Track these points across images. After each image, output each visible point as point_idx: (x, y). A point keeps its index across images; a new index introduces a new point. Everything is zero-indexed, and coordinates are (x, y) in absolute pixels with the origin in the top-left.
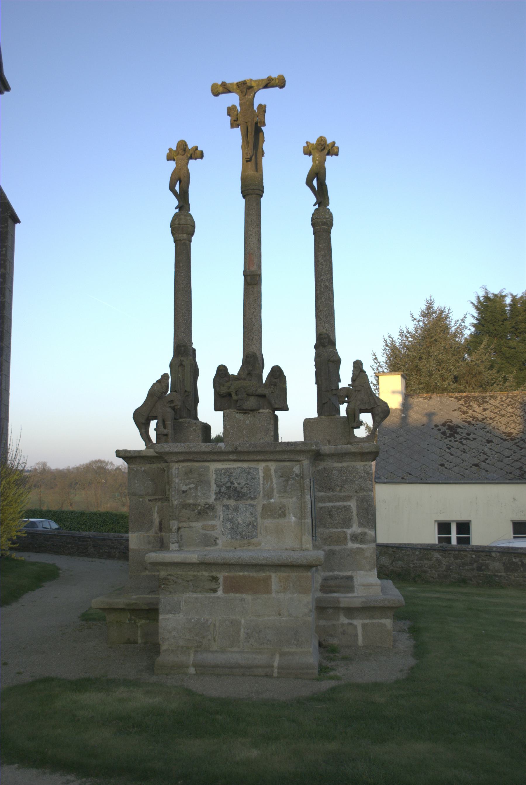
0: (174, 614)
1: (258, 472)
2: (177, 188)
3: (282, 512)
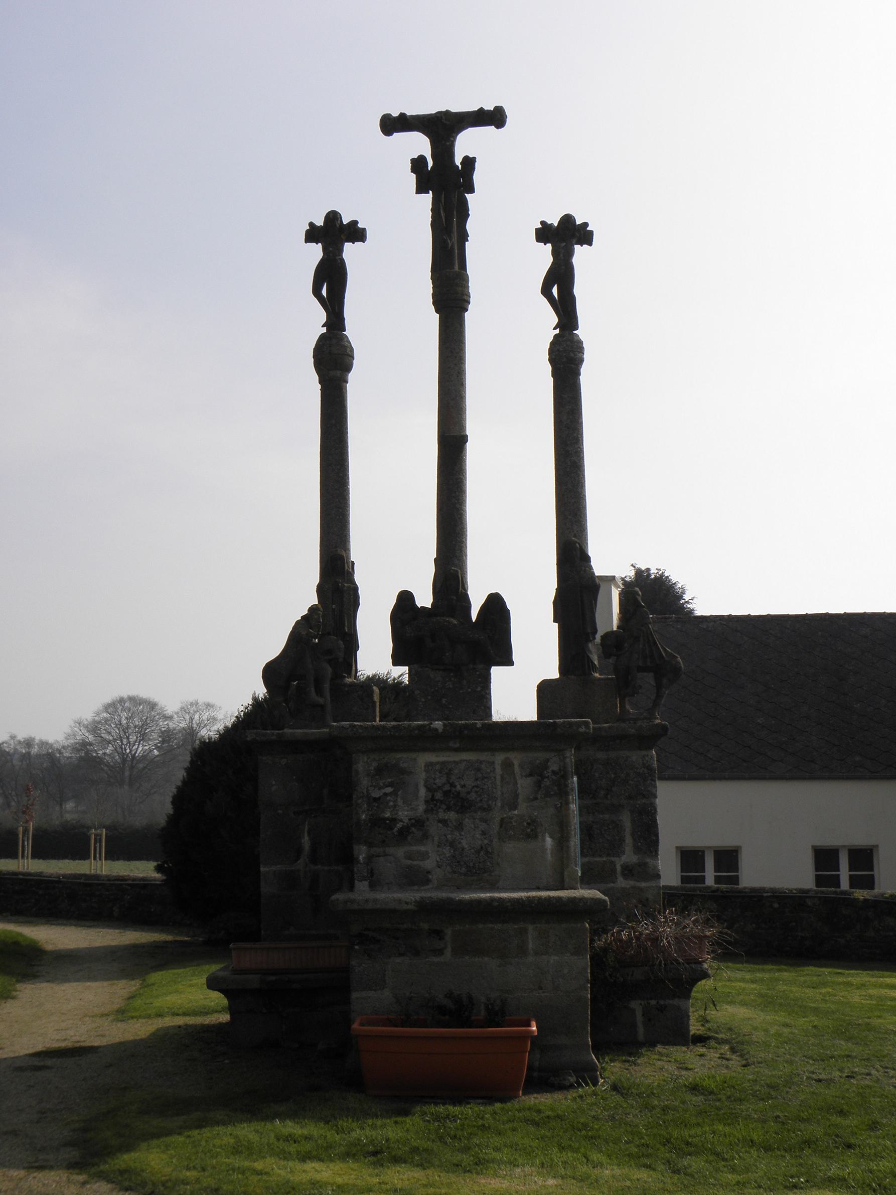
0: (375, 990)
1: (495, 769)
2: (324, 292)
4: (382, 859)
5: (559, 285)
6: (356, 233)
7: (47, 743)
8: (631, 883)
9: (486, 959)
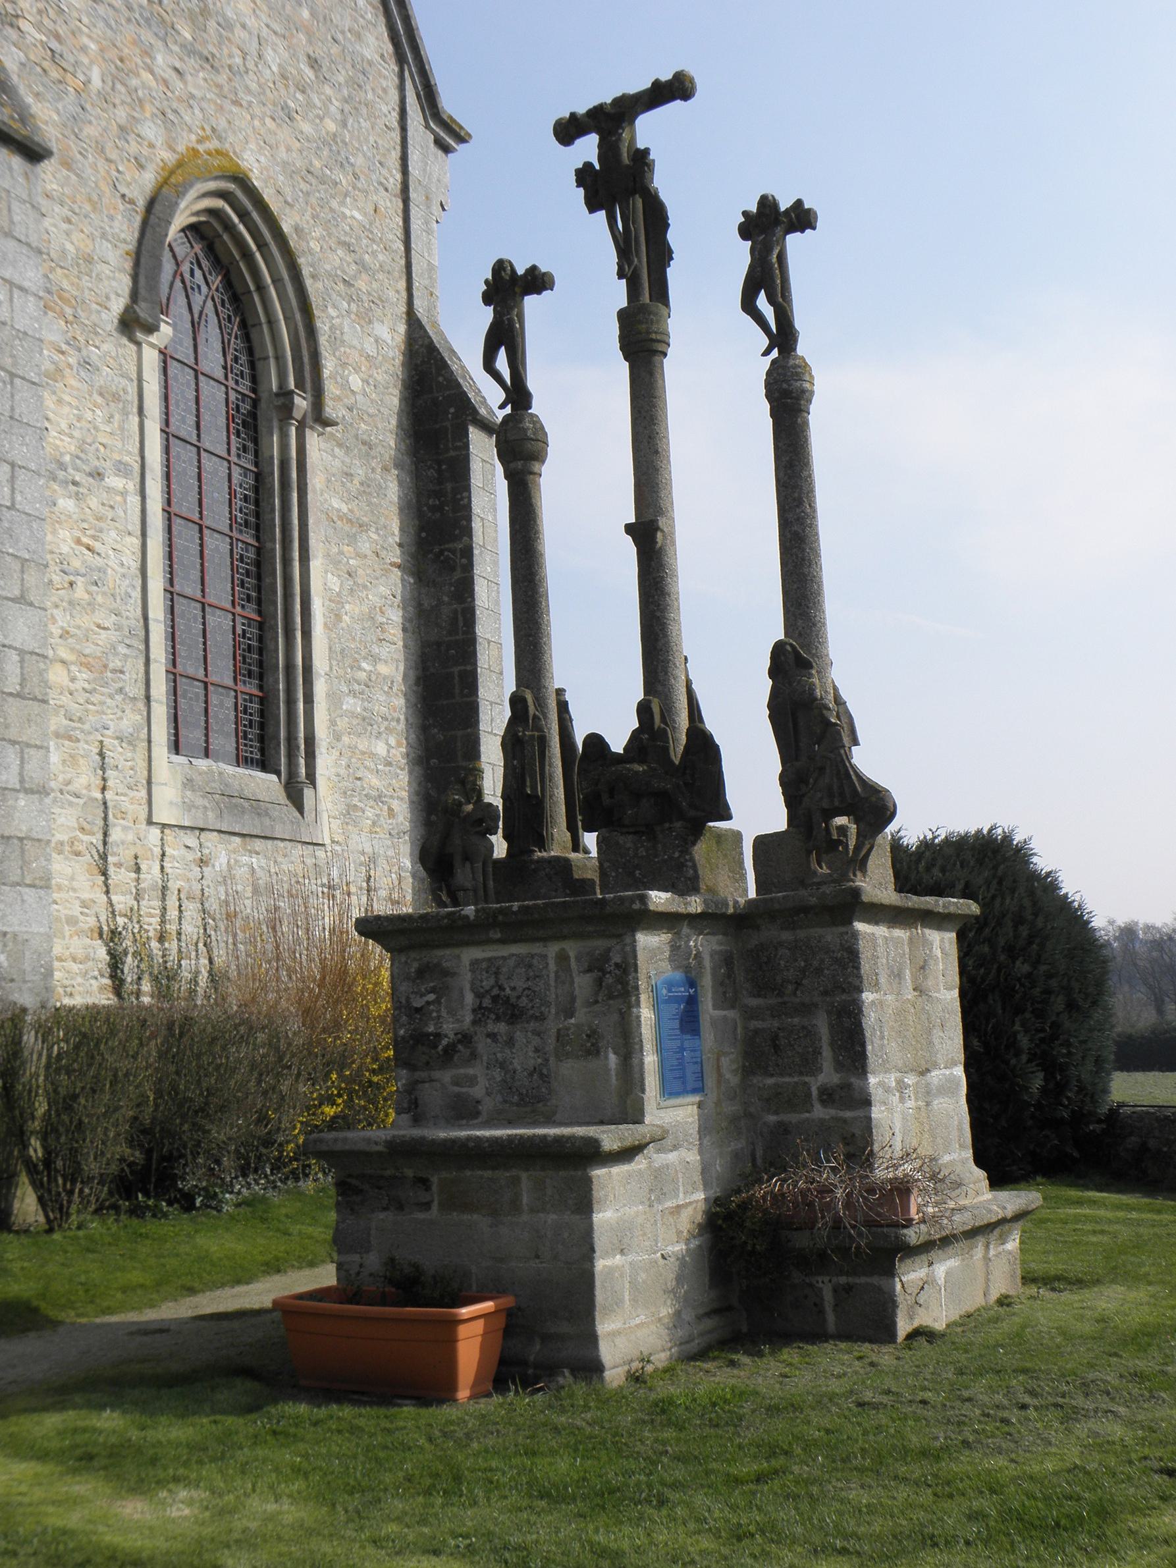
3: (593, 1045)
4: (427, 1085)
7: (1154, 927)
8: (833, 1112)
9: (475, 1216)
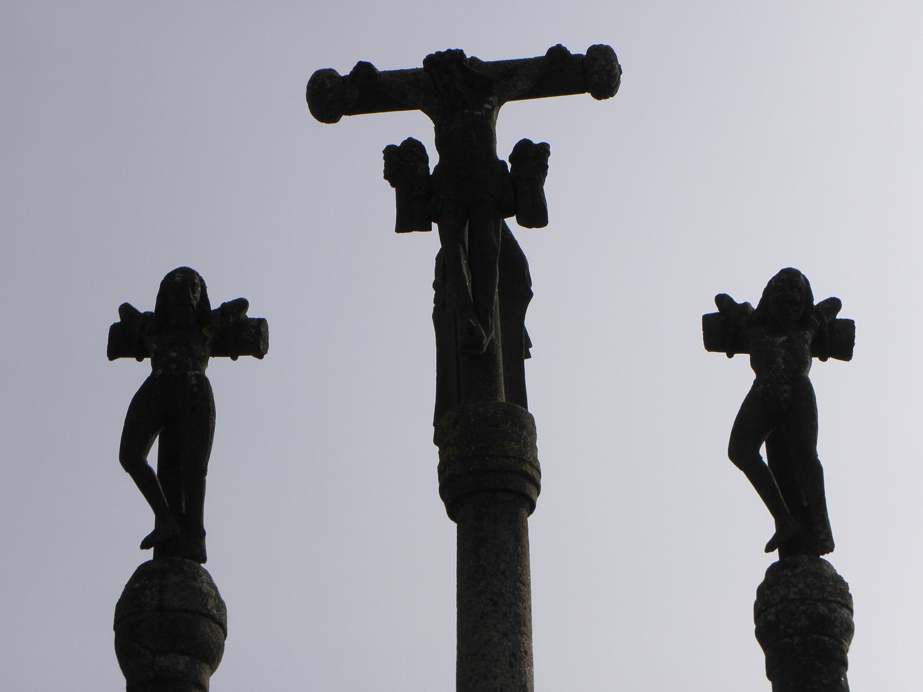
2: (152, 459)
5: (778, 445)
6: (242, 334)
